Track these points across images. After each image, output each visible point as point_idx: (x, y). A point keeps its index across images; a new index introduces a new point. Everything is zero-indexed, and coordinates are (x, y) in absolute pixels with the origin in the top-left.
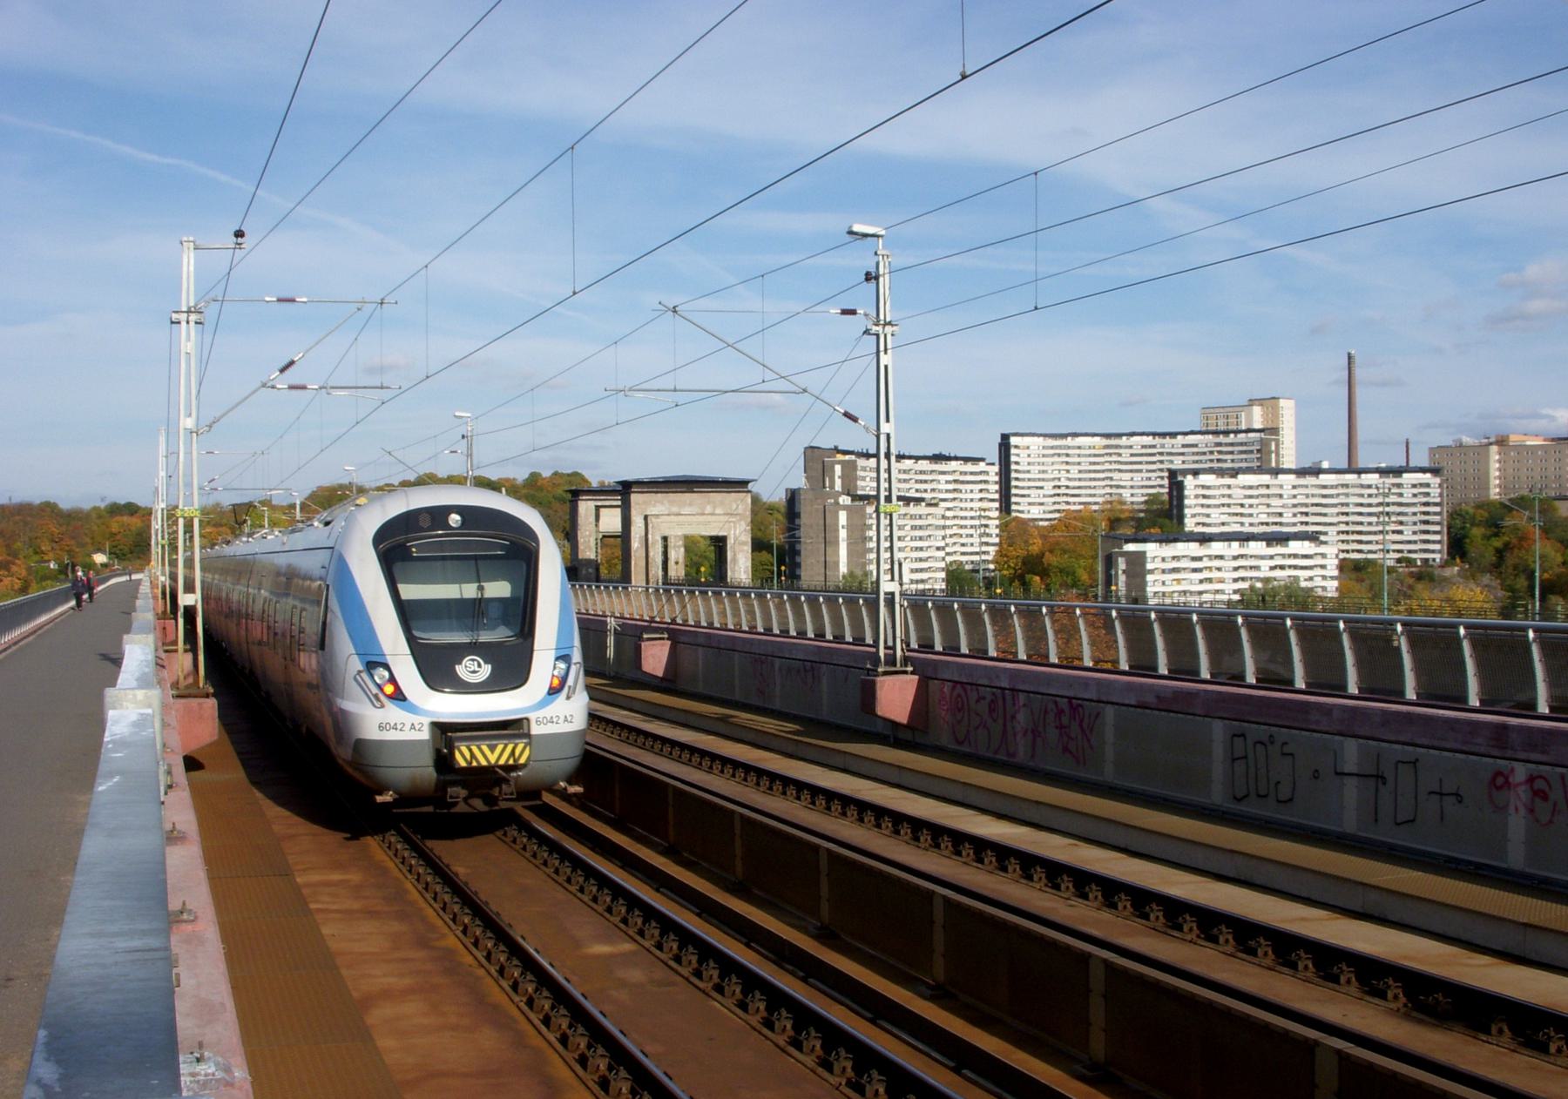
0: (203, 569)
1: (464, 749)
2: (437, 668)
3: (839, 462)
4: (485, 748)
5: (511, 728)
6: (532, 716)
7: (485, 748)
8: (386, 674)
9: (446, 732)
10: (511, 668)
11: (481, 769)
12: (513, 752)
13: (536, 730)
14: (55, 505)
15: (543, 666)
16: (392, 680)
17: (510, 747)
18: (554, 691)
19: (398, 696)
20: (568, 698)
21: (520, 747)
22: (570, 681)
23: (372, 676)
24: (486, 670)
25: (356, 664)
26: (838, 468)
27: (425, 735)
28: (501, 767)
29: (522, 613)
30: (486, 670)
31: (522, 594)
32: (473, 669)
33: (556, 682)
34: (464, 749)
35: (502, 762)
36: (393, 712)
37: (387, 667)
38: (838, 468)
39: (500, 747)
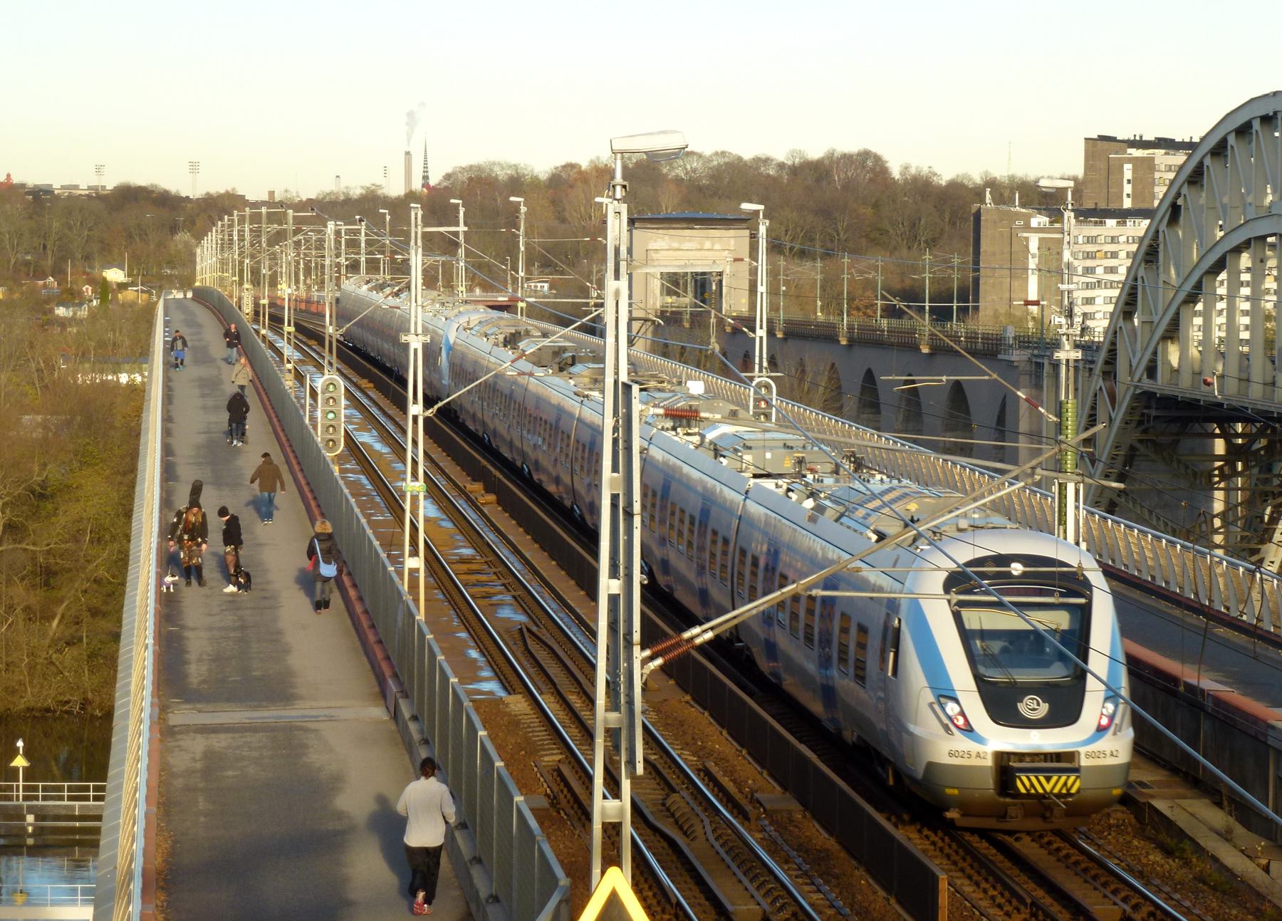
0: (824, 599)
1: (1024, 779)
2: (1002, 705)
3: (1130, 160)
4: (1042, 779)
5: (1062, 761)
6: (1083, 750)
7: (1042, 779)
8: (957, 709)
9: (1006, 766)
10: (1065, 708)
11: (1038, 796)
12: (1065, 784)
13: (1084, 762)
14: (867, 167)
15: (1095, 707)
16: (962, 714)
17: (1063, 778)
18: (1101, 730)
19: (968, 730)
20: (1115, 734)
21: (1072, 778)
22: (1117, 720)
23: (943, 709)
24: (1044, 709)
25: (929, 696)
26: (1128, 168)
27: (989, 762)
28: (1056, 795)
29: (1079, 638)
30: (1044, 709)
31: (1077, 627)
32: (1034, 707)
33: (1104, 721)
34: (1024, 779)
35: (1056, 791)
36: (961, 743)
37: (956, 701)
38: (1128, 168)
39: (1055, 778)
